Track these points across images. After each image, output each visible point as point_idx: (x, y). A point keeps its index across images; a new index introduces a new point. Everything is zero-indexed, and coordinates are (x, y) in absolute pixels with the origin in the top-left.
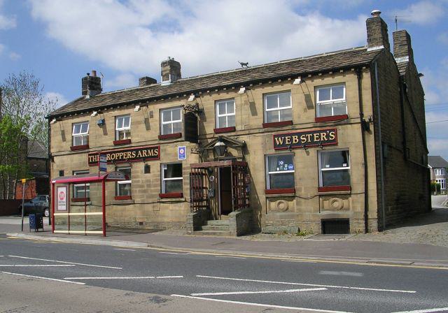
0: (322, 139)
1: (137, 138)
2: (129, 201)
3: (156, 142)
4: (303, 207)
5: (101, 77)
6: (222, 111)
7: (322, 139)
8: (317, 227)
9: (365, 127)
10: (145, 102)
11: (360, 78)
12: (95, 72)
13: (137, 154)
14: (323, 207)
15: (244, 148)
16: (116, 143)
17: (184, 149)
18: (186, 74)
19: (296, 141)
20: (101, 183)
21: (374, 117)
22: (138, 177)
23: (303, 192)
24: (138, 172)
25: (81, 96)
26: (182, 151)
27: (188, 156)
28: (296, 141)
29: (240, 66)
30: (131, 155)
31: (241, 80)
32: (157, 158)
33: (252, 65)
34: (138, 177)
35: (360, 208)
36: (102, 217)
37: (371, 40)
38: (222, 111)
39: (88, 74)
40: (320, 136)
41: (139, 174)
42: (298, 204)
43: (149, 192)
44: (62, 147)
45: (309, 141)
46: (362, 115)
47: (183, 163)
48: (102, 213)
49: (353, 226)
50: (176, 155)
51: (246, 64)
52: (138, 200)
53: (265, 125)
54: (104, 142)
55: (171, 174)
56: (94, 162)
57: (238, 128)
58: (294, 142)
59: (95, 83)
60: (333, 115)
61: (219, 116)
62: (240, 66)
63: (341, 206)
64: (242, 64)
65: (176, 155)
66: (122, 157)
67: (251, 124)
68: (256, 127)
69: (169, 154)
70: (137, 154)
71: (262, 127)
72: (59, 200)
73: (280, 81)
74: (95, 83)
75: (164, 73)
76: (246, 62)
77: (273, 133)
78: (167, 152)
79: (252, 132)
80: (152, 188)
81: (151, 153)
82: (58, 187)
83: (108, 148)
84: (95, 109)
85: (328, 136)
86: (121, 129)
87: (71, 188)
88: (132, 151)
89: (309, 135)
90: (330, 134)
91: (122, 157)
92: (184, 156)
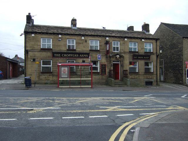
1: (79, 49)
4: (140, 78)
8: (144, 84)
18: (79, 25)
26: (99, 57)
29: (102, 28)
31: (127, 35)
35: (155, 78)
40: (74, 55)
44: (34, 48)
46: (157, 53)
48: (91, 79)
50: (97, 58)
51: (105, 28)
53: (130, 52)
56: (57, 57)
61: (113, 46)
62: (102, 28)
64: (103, 28)
66: (72, 56)
67: (125, 50)
72: (62, 73)
79: (124, 53)
80: (86, 69)
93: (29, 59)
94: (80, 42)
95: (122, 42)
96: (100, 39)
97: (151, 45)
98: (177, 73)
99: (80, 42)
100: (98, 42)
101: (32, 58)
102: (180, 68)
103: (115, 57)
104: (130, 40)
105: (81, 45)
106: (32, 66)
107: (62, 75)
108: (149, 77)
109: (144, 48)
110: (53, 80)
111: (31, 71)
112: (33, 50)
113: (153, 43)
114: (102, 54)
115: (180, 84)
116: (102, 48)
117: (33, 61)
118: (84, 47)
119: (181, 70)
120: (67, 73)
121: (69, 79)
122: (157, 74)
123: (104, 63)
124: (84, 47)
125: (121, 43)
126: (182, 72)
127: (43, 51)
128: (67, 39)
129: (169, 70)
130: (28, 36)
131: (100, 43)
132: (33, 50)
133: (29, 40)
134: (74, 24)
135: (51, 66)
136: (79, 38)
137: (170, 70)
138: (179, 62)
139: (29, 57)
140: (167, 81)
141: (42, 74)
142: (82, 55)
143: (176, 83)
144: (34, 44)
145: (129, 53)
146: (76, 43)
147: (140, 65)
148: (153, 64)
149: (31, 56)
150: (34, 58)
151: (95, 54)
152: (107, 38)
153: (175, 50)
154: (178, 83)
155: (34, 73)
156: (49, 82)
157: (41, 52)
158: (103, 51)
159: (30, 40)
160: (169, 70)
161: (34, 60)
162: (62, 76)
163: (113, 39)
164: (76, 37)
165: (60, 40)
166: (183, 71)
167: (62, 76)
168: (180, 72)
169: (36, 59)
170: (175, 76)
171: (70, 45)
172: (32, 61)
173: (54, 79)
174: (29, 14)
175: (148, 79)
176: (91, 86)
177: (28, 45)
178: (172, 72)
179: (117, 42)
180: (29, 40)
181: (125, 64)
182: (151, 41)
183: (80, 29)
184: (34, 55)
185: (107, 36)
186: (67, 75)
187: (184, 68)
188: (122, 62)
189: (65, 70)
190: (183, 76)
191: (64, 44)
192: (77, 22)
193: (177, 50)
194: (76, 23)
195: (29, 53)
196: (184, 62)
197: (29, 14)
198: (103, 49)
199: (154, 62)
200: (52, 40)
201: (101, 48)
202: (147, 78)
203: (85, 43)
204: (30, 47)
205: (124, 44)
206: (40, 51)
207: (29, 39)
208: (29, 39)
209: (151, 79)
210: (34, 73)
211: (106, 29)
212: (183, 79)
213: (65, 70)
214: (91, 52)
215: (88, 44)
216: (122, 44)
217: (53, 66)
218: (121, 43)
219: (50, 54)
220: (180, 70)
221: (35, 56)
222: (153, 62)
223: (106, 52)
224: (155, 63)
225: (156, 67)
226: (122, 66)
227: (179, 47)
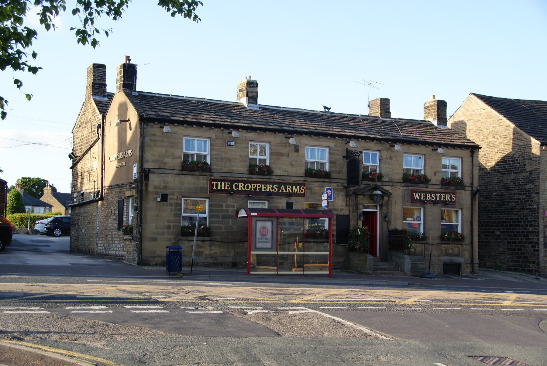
0: (447, 200)
3: (247, 176)
7: (268, 190)
9: (473, 194)
13: (279, 188)
17: (331, 190)
19: (429, 198)
28: (429, 198)
30: (273, 188)
33: (335, 109)
35: (467, 254)
44: (165, 163)
45: (438, 199)
51: (329, 109)
54: (235, 169)
55: (455, 227)
58: (427, 199)
62: (323, 110)
64: (325, 107)
66: (255, 189)
67: (394, 177)
68: (397, 181)
69: (315, 193)
70: (279, 188)
72: (258, 235)
76: (329, 107)
77: (411, 188)
78: (313, 191)
79: (391, 184)
81: (296, 189)
82: (257, 220)
83: (241, 176)
85: (451, 198)
88: (273, 183)
89: (438, 195)
90: (452, 196)
92: (331, 198)
93: (151, 196)
94: (282, 151)
95: (385, 154)
96: (332, 143)
97: (323, 151)
98: (520, 242)
99: (284, 150)
100: (327, 150)
101: (157, 193)
102: (531, 229)
103: (369, 193)
104: (406, 147)
105: (284, 158)
106: (158, 216)
107: (257, 240)
108: (450, 251)
109: (440, 172)
110: (210, 255)
111: (156, 228)
112: (162, 170)
113: (464, 159)
114: (335, 185)
115: (530, 272)
116: (337, 169)
117: (162, 200)
118: (292, 165)
119: (533, 232)
120: (269, 236)
121: (275, 253)
122: (472, 243)
123: (342, 210)
124: (292, 165)
125: (384, 156)
126: (534, 241)
127: (187, 173)
128: (307, 145)
129: (494, 232)
130: (153, 129)
131: (330, 154)
132: (161, 171)
133: (151, 140)
134: (250, 95)
135: (206, 215)
136: (279, 138)
137: (498, 233)
138: (526, 211)
139: (151, 188)
140: (488, 264)
141: (184, 238)
142: (289, 188)
143: (516, 270)
144: (164, 151)
145: (403, 184)
146: (271, 154)
147: (429, 218)
148: (462, 215)
149: (155, 187)
150: (165, 192)
151: (319, 184)
152: (352, 144)
153: (513, 176)
154: (524, 271)
155: (163, 234)
156: (201, 259)
157: (183, 176)
158: (340, 176)
159: (155, 141)
160: (493, 232)
161: (164, 198)
162: (259, 245)
163: (363, 144)
164: (271, 137)
165: (232, 143)
166: (538, 236)
167: (259, 245)
168: (529, 239)
169: (169, 197)
170: (514, 250)
171: (256, 159)
172: (159, 199)
173: (215, 253)
174: (34, 52)
175: (451, 255)
176: (328, 272)
177: (148, 155)
178: (505, 239)
179: (261, 144)
180: (151, 140)
181: (393, 214)
182: (459, 152)
183: (265, 109)
184: (163, 185)
185: (350, 137)
186: (270, 241)
187: (541, 229)
188: (384, 209)
189: (266, 229)
190: (538, 250)
191: (241, 156)
192: (260, 89)
193: (521, 176)
194: (257, 93)
195: (152, 177)
196: (541, 211)
197: (34, 52)
198: (339, 172)
199: (465, 210)
200: (212, 145)
201: (333, 169)
202: (447, 255)
203: (293, 155)
204: (154, 161)
205: (391, 158)
206: (180, 172)
207: (153, 138)
208: (153, 138)
209: (455, 255)
210: (163, 234)
211: (331, 111)
212: (538, 258)
213: (264, 228)
214: (309, 179)
215: (302, 157)
216: (386, 158)
217: (211, 216)
218: (384, 156)
219: (205, 181)
220: (529, 232)
221: (166, 188)
222: (461, 209)
223: (346, 181)
224: (467, 214)
225: (469, 223)
226: (386, 217)
227: (528, 168)
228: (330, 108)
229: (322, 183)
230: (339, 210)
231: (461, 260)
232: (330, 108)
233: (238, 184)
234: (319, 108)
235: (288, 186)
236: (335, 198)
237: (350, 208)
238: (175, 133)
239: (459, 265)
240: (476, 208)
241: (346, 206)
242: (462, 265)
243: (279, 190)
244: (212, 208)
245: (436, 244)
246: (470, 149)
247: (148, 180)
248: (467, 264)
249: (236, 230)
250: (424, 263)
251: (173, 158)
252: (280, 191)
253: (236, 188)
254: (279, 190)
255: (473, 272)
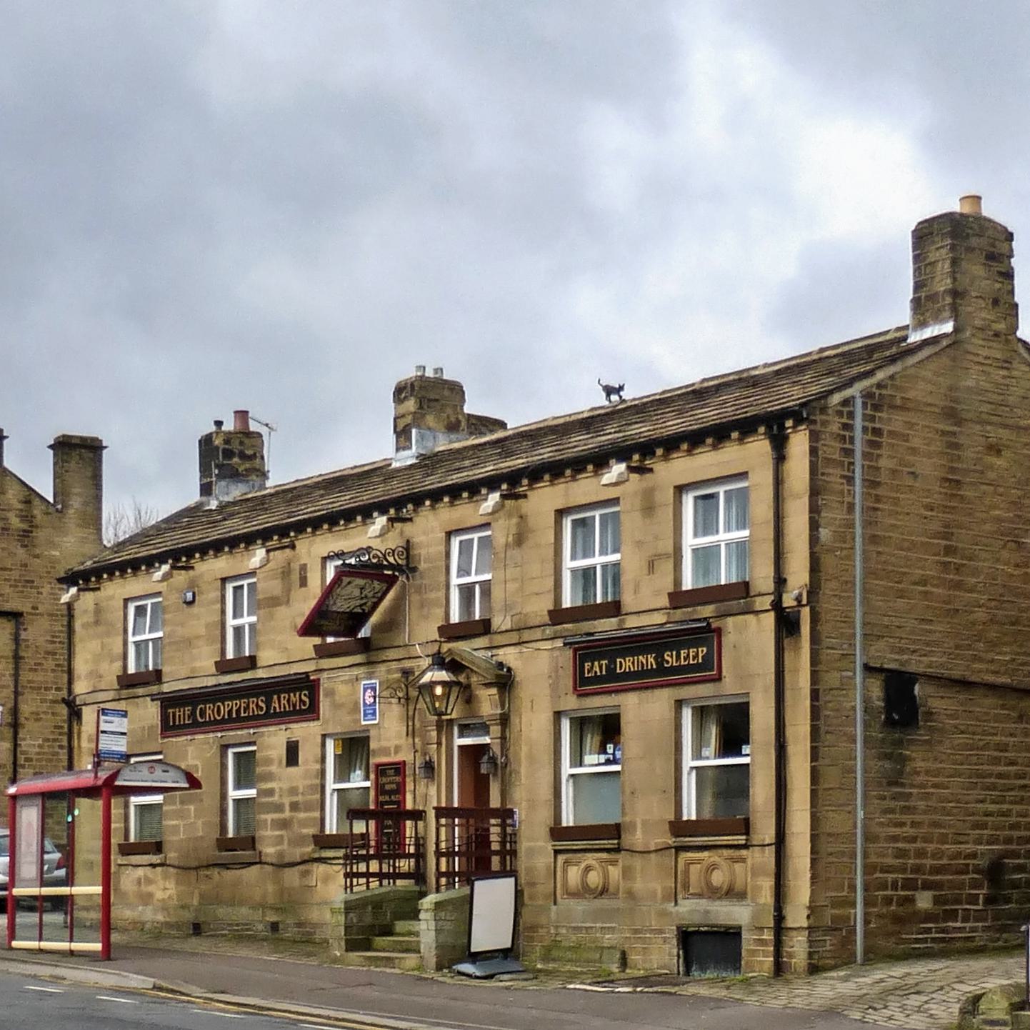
2: (246, 855)
5: (264, 431)
6: (706, 524)
9: (786, 624)
10: (286, 535)
11: (780, 457)
12: (242, 415)
14: (686, 886)
15: (504, 681)
16: (224, 666)
17: (374, 689)
20: (99, 803)
21: (809, 593)
22: (269, 777)
23: (639, 834)
24: (268, 761)
25: (193, 497)
27: (382, 715)
30: (257, 705)
32: (311, 712)
34: (269, 777)
36: (100, 901)
37: (923, 306)
38: (706, 524)
39: (219, 424)
41: (274, 768)
42: (627, 873)
43: (296, 827)
47: (373, 733)
48: (99, 889)
49: (759, 958)
52: (269, 850)
57: (500, 622)
59: (243, 456)
60: (723, 582)
63: (725, 887)
64: (609, 391)
65: (356, 708)
67: (528, 609)
71: (547, 619)
73: (735, 435)
74: (243, 456)
75: (402, 424)
84: (382, 508)
86: (238, 622)
87: (116, 812)
91: (238, 711)
92: (374, 714)
123: (397, 749)
181: (524, 749)
216: (507, 545)
228: (621, 388)
229: (354, 668)
230: (392, 750)
231: (736, 914)
232: (621, 388)
233: (205, 707)
234: (590, 400)
235: (282, 696)
236: (382, 715)
237: (417, 740)
238: (962, 581)
239: (731, 935)
240: (801, 685)
241: (407, 735)
242: (745, 935)
243: (268, 708)
244: (920, 886)
245: (656, 851)
246: (762, 429)
247: (81, 724)
248: (761, 929)
249: (201, 834)
250: (613, 928)
251: (111, 661)
252: (272, 711)
253: (202, 718)
254: (268, 708)
255: (779, 968)
